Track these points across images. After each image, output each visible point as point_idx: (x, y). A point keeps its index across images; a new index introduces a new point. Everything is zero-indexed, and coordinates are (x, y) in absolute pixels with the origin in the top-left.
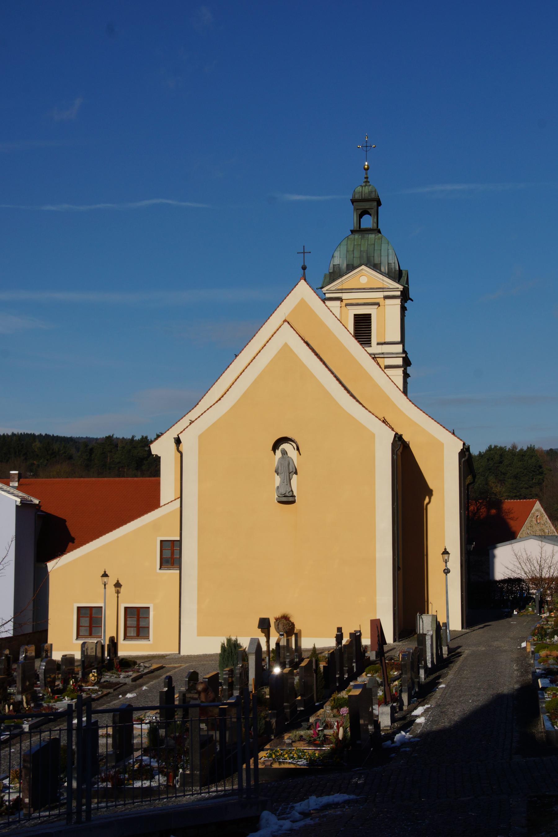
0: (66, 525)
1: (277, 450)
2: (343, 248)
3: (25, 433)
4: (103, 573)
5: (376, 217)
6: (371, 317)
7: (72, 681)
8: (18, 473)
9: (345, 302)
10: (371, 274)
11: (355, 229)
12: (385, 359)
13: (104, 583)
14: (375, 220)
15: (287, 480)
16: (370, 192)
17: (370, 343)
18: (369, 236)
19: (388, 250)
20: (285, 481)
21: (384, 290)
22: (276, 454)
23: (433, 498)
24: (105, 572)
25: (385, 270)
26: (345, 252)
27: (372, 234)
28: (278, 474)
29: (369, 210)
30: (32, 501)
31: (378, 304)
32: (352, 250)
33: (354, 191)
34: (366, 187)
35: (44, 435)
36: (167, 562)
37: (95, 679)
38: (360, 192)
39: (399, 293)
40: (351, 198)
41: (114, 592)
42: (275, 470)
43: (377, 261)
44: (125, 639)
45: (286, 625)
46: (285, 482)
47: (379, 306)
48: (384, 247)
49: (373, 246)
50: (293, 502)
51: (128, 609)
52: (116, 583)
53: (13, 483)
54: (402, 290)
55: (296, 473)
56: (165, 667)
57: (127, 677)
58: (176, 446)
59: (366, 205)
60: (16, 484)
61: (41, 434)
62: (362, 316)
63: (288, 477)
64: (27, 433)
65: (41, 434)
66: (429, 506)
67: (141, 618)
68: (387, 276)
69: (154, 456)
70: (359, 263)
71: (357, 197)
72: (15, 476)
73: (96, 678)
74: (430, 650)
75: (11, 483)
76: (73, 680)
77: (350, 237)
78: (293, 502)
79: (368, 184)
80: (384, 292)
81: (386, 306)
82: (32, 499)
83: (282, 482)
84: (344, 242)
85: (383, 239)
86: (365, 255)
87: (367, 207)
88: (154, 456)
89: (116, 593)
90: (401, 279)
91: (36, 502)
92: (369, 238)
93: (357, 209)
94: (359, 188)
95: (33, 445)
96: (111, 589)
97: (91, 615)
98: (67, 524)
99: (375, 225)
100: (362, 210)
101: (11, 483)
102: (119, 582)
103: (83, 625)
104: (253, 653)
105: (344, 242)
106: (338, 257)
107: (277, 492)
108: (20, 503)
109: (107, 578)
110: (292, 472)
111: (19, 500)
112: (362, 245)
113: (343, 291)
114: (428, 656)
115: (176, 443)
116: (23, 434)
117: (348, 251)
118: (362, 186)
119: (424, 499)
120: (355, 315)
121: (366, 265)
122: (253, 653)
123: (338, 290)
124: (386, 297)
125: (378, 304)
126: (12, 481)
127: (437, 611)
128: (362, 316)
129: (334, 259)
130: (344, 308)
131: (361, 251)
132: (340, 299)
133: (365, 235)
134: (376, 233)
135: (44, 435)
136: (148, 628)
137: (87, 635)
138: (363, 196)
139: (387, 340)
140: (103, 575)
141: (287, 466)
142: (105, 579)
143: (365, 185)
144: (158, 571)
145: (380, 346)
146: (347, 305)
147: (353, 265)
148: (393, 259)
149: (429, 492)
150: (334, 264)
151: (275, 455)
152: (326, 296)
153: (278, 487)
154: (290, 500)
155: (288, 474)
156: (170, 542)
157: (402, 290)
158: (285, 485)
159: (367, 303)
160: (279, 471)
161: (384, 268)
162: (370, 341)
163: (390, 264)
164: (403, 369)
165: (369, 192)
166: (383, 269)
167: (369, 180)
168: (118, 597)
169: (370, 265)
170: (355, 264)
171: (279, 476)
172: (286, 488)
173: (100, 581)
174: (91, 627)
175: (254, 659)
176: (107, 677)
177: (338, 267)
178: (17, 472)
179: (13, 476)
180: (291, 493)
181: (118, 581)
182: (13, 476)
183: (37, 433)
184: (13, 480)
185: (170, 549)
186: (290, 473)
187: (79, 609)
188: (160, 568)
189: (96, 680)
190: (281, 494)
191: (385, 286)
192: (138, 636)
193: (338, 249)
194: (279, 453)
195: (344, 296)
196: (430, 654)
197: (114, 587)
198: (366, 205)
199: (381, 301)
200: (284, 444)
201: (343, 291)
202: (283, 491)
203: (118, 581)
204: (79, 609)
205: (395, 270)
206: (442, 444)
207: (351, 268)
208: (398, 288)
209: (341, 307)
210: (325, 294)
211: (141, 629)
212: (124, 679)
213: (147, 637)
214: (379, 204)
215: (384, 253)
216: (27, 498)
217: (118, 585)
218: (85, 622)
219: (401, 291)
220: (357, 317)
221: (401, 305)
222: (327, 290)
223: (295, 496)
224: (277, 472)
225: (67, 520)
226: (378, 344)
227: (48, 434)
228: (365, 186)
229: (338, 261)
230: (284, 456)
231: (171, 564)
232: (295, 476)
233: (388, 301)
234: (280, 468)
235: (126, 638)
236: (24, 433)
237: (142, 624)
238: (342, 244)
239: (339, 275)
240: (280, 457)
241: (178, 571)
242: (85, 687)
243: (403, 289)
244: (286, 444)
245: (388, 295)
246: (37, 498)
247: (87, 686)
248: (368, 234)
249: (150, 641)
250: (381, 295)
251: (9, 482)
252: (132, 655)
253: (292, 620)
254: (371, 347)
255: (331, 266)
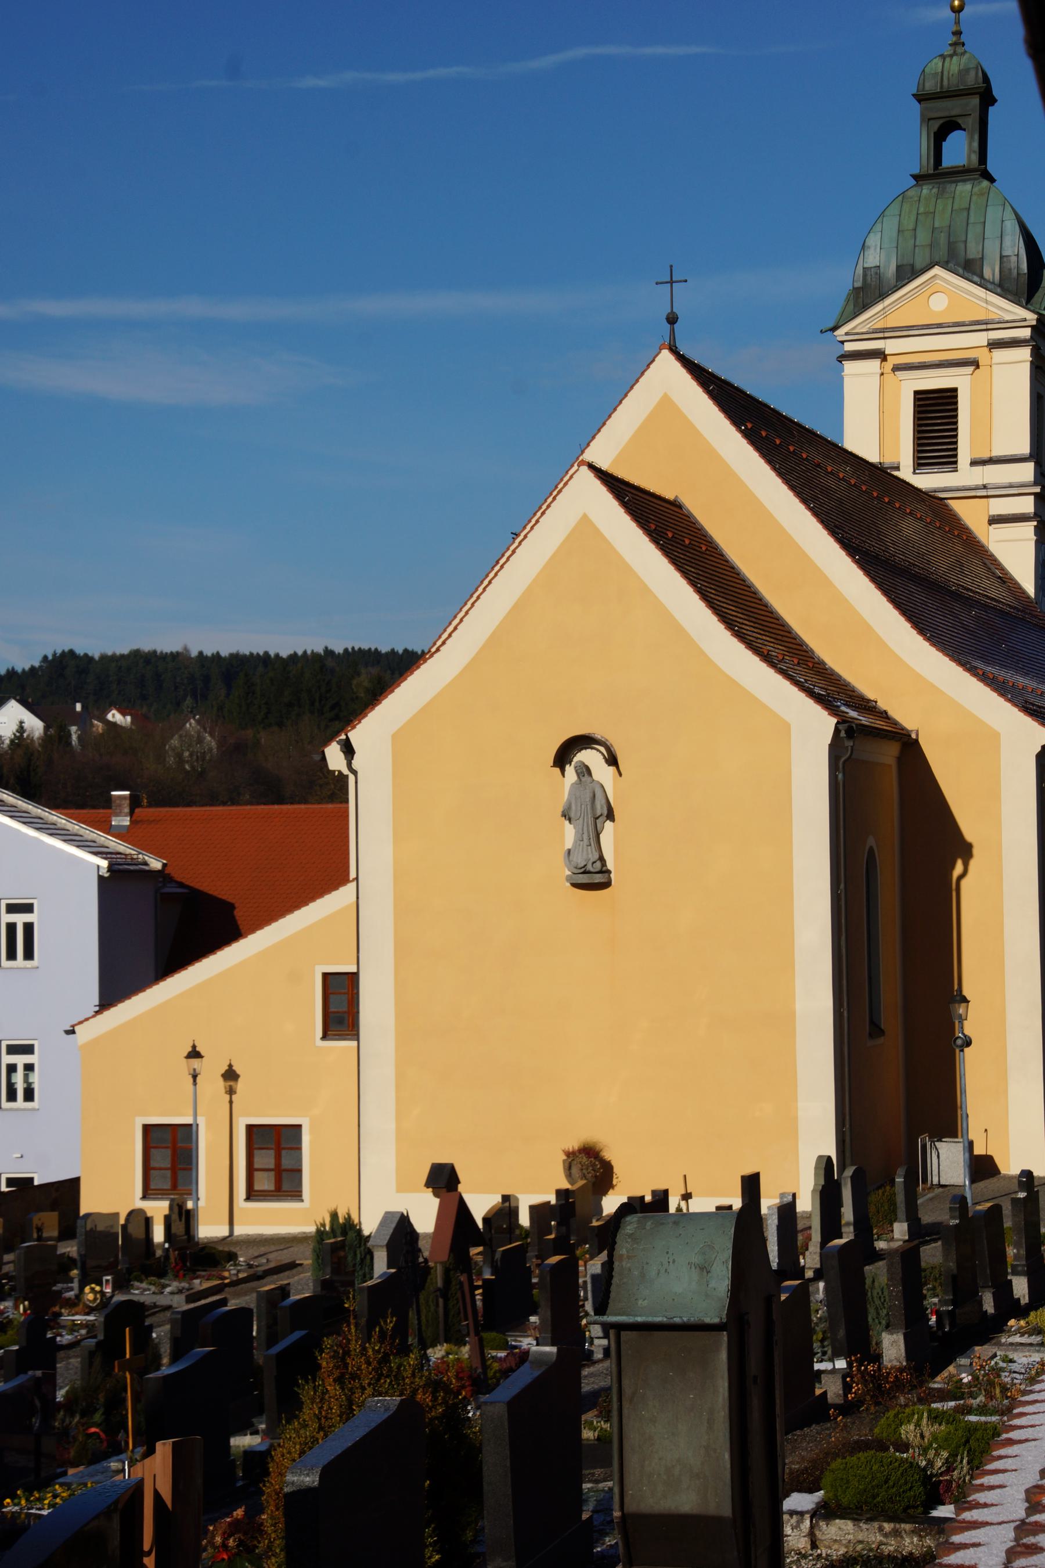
0: (233, 917)
1: (567, 767)
2: (890, 224)
3: (356, 648)
4: (190, 1049)
5: (976, 137)
6: (956, 397)
7: (24, 1306)
8: (130, 794)
9: (891, 361)
10: (957, 287)
11: (924, 171)
12: (991, 500)
13: (192, 1072)
14: (976, 145)
15: (589, 836)
16: (964, 72)
17: (956, 462)
18: (958, 188)
19: (1003, 221)
20: (585, 836)
21: (990, 327)
22: (566, 773)
23: (973, 863)
24: (194, 1047)
25: (993, 275)
26: (895, 234)
27: (964, 181)
28: (570, 820)
29: (960, 121)
30: (146, 864)
31: (975, 364)
32: (911, 226)
33: (924, 71)
34: (955, 58)
35: (401, 652)
36: (340, 1021)
37: (95, 1299)
38: (936, 74)
39: (1026, 333)
40: (915, 91)
41: (223, 1091)
42: (563, 812)
43: (973, 252)
44: (249, 1198)
45: (587, 1169)
46: (585, 839)
47: (978, 367)
48: (993, 213)
49: (965, 214)
50: (606, 885)
51: (255, 1129)
52: (226, 1071)
53: (119, 818)
54: (1034, 323)
55: (610, 816)
56: (301, 1265)
57: (177, 1293)
58: (346, 759)
59: (951, 108)
60: (126, 821)
61: (393, 650)
62: (936, 395)
63: (591, 828)
64: (360, 649)
65: (393, 650)
66: (964, 883)
67: (155, 1169)
68: (999, 290)
69: (337, 773)
70: (928, 261)
71: (930, 86)
72: (124, 802)
73: (98, 1296)
74: (776, 1238)
75: (113, 818)
76: (26, 1303)
77: (910, 193)
78: (606, 885)
79: (960, 49)
80: (990, 332)
81: (994, 367)
82: (146, 858)
83: (579, 839)
84: (894, 209)
85: (991, 195)
86: (943, 239)
87: (954, 113)
88: (337, 773)
89: (226, 1093)
90: (1037, 295)
91: (156, 864)
92: (957, 192)
93: (929, 119)
94: (936, 64)
95: (355, 682)
96: (212, 1084)
97: (174, 1142)
98: (238, 913)
99: (975, 158)
100: (941, 121)
101: (113, 818)
102: (234, 1068)
103: (157, 1166)
104: (382, 1246)
105: (894, 209)
106: (876, 246)
107: (568, 863)
108: (108, 871)
109: (200, 1059)
110: (601, 815)
111: (104, 864)
112: (937, 214)
113: (887, 335)
114: (773, 1251)
115: (343, 752)
116: (350, 650)
117: (903, 231)
118: (943, 57)
119: (953, 866)
120: (916, 393)
121: (945, 266)
122: (382, 1246)
123: (875, 331)
124: (995, 345)
125: (975, 364)
126: (117, 815)
127: (986, 1130)
128: (936, 395)
129: (866, 253)
130: (890, 377)
131: (934, 229)
132: (880, 355)
133: (948, 186)
134: (975, 179)
135: (401, 652)
136: (299, 1171)
137: (165, 1187)
138: (945, 82)
139: (997, 452)
140: (190, 1053)
141: (589, 804)
142: (195, 1063)
143: (951, 52)
144: (140, 1121)
145: (979, 469)
146: (896, 368)
147: (912, 266)
148: (1015, 246)
149: (966, 851)
150: (865, 266)
151: (564, 776)
152: (846, 349)
153: (569, 851)
154: (596, 881)
155: (591, 821)
156: (346, 976)
157: (1034, 323)
158: (585, 846)
159: (947, 360)
160: (572, 815)
161: (993, 270)
162: (956, 456)
163: (1005, 259)
164: (1035, 523)
165: (960, 71)
166: (987, 273)
167: (963, 38)
168: (231, 1102)
169: (957, 264)
170: (919, 265)
171: (572, 826)
172: (588, 854)
173: (184, 1067)
174: (174, 1170)
175: (385, 1259)
176: (136, 1292)
177: (876, 273)
178: (127, 793)
179: (118, 802)
180: (598, 865)
181: (230, 1066)
182: (118, 802)
183: (384, 649)
184: (118, 811)
185: (344, 993)
186: (598, 818)
187: (147, 1129)
188: (325, 1037)
189: (98, 1301)
190: (576, 868)
191: (992, 316)
192: (279, 1191)
193: (878, 226)
194: (570, 770)
195: (890, 346)
196: (777, 1248)
197: (221, 1080)
198: (951, 108)
199: (983, 355)
200: (584, 751)
201: (887, 335)
202: (579, 860)
203: (230, 1066)
204: (147, 1129)
205: (1018, 274)
206: (995, 736)
207: (907, 273)
208: (1025, 320)
209: (882, 374)
210: (842, 342)
211: (284, 1175)
212: (171, 1297)
213: (296, 1194)
214: (987, 98)
215: (991, 231)
216: (135, 857)
217: (230, 1075)
218: (162, 1158)
219: (1032, 327)
220: (920, 396)
221: (1031, 362)
222: (847, 334)
223: (609, 872)
224: (566, 815)
225: (236, 905)
226: (974, 463)
227: (410, 649)
228: (951, 56)
229: (875, 258)
230: (583, 779)
231: (349, 1026)
232: (608, 824)
233: (999, 355)
234: (573, 807)
235: (252, 1194)
236: (353, 648)
237: (286, 1163)
238: (886, 213)
239: (877, 294)
240: (574, 782)
241: (355, 1043)
242: (69, 1315)
243: (1038, 320)
244: (589, 750)
245: (999, 339)
246: (158, 854)
247: (73, 1315)
248: (956, 182)
249: (302, 1201)
250: (981, 339)
251: (110, 817)
252: (265, 1233)
253: (607, 1155)
254: (957, 471)
255: (860, 271)
